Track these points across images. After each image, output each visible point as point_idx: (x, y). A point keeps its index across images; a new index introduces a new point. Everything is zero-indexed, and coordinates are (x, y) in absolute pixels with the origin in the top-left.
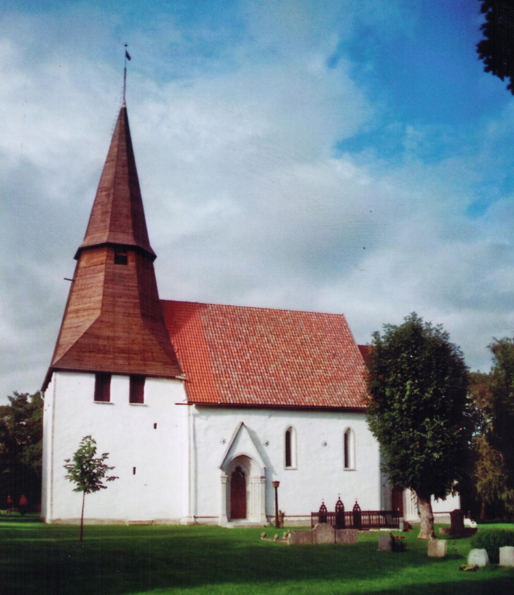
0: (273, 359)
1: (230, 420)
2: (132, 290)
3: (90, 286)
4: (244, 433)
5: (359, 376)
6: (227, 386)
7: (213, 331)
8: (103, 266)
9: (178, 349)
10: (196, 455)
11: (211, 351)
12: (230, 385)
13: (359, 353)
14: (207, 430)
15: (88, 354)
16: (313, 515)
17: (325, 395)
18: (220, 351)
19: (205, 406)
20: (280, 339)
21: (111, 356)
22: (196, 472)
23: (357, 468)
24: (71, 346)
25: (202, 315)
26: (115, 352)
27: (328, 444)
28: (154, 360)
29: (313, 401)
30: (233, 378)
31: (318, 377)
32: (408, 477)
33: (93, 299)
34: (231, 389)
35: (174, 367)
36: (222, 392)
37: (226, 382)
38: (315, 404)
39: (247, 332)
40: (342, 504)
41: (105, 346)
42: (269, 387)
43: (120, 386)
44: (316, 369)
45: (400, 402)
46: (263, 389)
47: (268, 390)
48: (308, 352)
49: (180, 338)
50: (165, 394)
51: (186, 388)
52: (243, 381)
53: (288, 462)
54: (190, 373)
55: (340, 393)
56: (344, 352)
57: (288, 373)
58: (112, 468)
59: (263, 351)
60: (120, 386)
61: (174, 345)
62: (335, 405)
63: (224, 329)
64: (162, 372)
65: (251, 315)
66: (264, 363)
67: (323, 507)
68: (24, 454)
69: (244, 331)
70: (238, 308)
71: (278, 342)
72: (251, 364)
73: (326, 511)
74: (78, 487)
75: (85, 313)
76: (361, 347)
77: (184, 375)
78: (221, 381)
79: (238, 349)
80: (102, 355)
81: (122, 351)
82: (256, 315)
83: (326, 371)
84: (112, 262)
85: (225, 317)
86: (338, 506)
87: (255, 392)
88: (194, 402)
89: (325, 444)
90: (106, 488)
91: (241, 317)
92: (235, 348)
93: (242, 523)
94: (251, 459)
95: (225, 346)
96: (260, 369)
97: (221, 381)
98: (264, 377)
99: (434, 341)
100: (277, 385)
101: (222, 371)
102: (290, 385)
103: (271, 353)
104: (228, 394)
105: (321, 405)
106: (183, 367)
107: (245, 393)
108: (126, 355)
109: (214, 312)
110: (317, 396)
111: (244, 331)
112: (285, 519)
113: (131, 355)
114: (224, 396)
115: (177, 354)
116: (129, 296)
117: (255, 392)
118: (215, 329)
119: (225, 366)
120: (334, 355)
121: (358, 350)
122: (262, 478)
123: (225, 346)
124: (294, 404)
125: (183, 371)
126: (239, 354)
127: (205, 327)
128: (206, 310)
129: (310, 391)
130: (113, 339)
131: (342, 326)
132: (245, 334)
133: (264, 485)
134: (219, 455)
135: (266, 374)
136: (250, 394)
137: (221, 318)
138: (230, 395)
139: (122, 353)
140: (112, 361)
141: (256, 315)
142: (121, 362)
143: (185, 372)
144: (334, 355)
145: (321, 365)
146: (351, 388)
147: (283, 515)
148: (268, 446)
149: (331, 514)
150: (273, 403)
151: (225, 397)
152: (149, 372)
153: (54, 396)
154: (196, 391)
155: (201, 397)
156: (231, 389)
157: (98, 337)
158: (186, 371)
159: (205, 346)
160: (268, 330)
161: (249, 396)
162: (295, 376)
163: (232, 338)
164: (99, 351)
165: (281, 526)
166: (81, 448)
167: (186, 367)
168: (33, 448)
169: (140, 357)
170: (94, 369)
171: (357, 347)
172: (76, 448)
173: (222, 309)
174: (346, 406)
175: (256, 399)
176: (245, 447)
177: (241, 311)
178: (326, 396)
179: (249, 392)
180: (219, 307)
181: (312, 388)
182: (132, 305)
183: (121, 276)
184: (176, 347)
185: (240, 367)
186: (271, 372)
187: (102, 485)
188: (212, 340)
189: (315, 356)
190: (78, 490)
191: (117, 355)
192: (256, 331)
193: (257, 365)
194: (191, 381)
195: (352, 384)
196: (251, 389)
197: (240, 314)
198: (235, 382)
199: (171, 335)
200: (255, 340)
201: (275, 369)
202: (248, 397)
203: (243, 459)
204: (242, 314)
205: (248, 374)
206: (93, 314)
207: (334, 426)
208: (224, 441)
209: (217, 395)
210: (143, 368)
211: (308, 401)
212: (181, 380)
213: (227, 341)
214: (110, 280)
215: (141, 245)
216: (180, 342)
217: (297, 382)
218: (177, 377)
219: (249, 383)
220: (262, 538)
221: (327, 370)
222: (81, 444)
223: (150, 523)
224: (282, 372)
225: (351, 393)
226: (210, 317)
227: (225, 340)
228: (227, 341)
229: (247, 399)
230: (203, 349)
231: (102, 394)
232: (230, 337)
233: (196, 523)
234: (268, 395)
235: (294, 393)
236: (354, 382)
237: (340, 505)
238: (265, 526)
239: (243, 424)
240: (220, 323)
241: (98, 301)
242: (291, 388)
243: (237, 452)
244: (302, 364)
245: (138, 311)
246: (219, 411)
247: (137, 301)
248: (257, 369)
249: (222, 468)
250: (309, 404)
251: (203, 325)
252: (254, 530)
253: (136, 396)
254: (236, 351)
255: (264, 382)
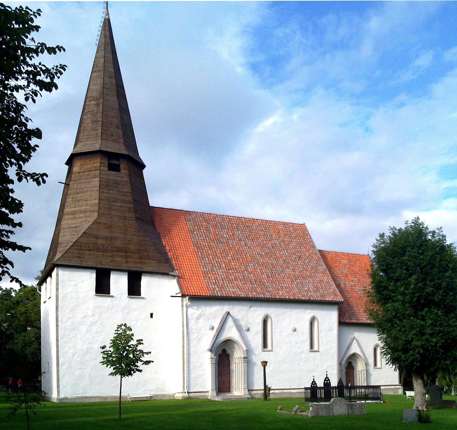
0: (250, 260)
1: (216, 311)
2: (127, 196)
3: (85, 190)
4: (230, 322)
5: (320, 274)
6: (214, 281)
7: (199, 235)
8: (98, 172)
9: (170, 250)
10: (188, 340)
11: (198, 252)
12: (217, 281)
13: (319, 256)
14: (198, 318)
15: (88, 252)
16: (306, 389)
17: (294, 290)
18: (206, 252)
19: (196, 299)
20: (255, 243)
21: (110, 254)
22: (189, 354)
23: (320, 350)
24: (71, 244)
25: (188, 221)
26: (113, 251)
27: (297, 330)
28: (149, 259)
29: (285, 294)
30: (219, 275)
31: (288, 275)
32: (409, 358)
33: (89, 202)
34: (217, 284)
35: (167, 265)
36: (211, 286)
37: (213, 278)
38: (287, 297)
39: (228, 236)
40: (329, 380)
41: (104, 245)
42: (249, 283)
43: (119, 282)
44: (286, 268)
45: (403, 294)
46: (244, 284)
47: (248, 285)
48: (278, 255)
49: (170, 240)
50: (159, 289)
51: (179, 282)
52: (227, 278)
53: (265, 345)
54: (181, 270)
55: (307, 288)
56: (307, 255)
57: (264, 271)
58: (147, 353)
59: (242, 253)
60: (119, 282)
61: (165, 246)
62: (303, 298)
63: (208, 234)
64: (157, 269)
65: (229, 222)
66: (243, 263)
67: (314, 383)
68: (16, 341)
69: (225, 236)
70: (218, 216)
71: (254, 246)
72: (233, 263)
73: (317, 386)
74: (114, 371)
75: (82, 215)
76: (319, 250)
77: (177, 272)
78: (209, 278)
79: (221, 250)
80: (101, 254)
81: (119, 250)
82: (233, 222)
83: (294, 270)
84: (107, 169)
85: (208, 223)
86: (326, 382)
87: (238, 287)
88: (187, 295)
89: (295, 330)
90: (140, 371)
91: (221, 224)
92: (218, 250)
93: (228, 395)
94: (236, 343)
95: (211, 248)
96: (241, 268)
97: (209, 278)
98: (244, 275)
99: (395, 246)
100: (255, 281)
101: (209, 269)
102: (266, 281)
103: (248, 255)
104: (215, 288)
105: (292, 298)
106: (175, 265)
107: (229, 288)
108: (124, 254)
109: (198, 219)
110: (288, 290)
111: (225, 236)
112: (271, 392)
113: (129, 254)
114: (212, 290)
115: (169, 253)
116: (124, 201)
117: (238, 287)
118: (200, 233)
119: (211, 265)
120: (300, 257)
121: (318, 253)
122: (244, 358)
123: (211, 248)
124: (270, 297)
125: (176, 268)
126: (223, 255)
127: (191, 231)
128: (190, 217)
129: (282, 286)
130: (111, 239)
131: (304, 233)
132: (226, 238)
133: (246, 364)
134: (207, 340)
135: (246, 272)
136: (234, 288)
137: (205, 224)
138: (217, 289)
139: (120, 252)
140: (111, 258)
141: (233, 222)
142: (118, 259)
143: (177, 270)
144: (300, 257)
145: (289, 265)
146: (315, 284)
147: (270, 389)
148: (249, 332)
149: (320, 388)
150: (253, 296)
151: (214, 290)
152: (145, 269)
153: (57, 289)
154: (189, 285)
155: (193, 291)
156: (217, 284)
157: (97, 237)
158: (178, 268)
159: (193, 247)
160: (245, 235)
161: (233, 290)
162: (269, 274)
163: (215, 242)
164: (98, 249)
165: (268, 398)
166: (116, 335)
167: (177, 265)
168: (25, 337)
169: (136, 256)
170: (94, 266)
171: (317, 251)
172: (112, 336)
173: (205, 217)
174: (312, 299)
175: (240, 293)
176: (230, 332)
177: (221, 218)
178: (296, 291)
179: (233, 287)
180: (202, 215)
181: (284, 284)
182: (128, 209)
183: (116, 183)
184: (168, 248)
185: (224, 266)
186: (250, 270)
187: (138, 368)
188: (199, 243)
189: (284, 258)
190: (115, 374)
191: (115, 253)
192: (234, 236)
193: (238, 264)
194: (183, 277)
195: (316, 281)
196: (234, 284)
197: (220, 221)
198: (221, 279)
199: (162, 237)
200: (235, 244)
201: (253, 268)
202: (232, 291)
203: (229, 342)
204: (222, 221)
205: (231, 271)
206: (90, 216)
207: (300, 316)
208: (213, 328)
209: (207, 289)
210: (139, 265)
211: (282, 294)
212: (174, 276)
213: (212, 244)
214: (104, 186)
215: (132, 155)
216: (171, 243)
217: (271, 279)
218: (170, 273)
219: (232, 279)
220: (278, 411)
221: (295, 269)
222: (117, 332)
223: (149, 399)
224: (259, 270)
225: (315, 289)
226: (195, 223)
227: (210, 243)
228: (212, 244)
229: (231, 292)
230: (192, 250)
231: (103, 288)
232: (214, 241)
233: (189, 398)
234: (249, 289)
235: (269, 287)
236: (317, 279)
237: (327, 381)
238: (248, 398)
239: (229, 313)
240: (204, 228)
241: (95, 205)
242: (267, 284)
243: (225, 336)
244: (274, 264)
245: (133, 215)
246: (208, 303)
247: (132, 205)
248: (238, 268)
249: (211, 350)
250: (282, 297)
251: (190, 229)
252: (239, 401)
253: (134, 290)
254: (219, 252)
255: (244, 278)
